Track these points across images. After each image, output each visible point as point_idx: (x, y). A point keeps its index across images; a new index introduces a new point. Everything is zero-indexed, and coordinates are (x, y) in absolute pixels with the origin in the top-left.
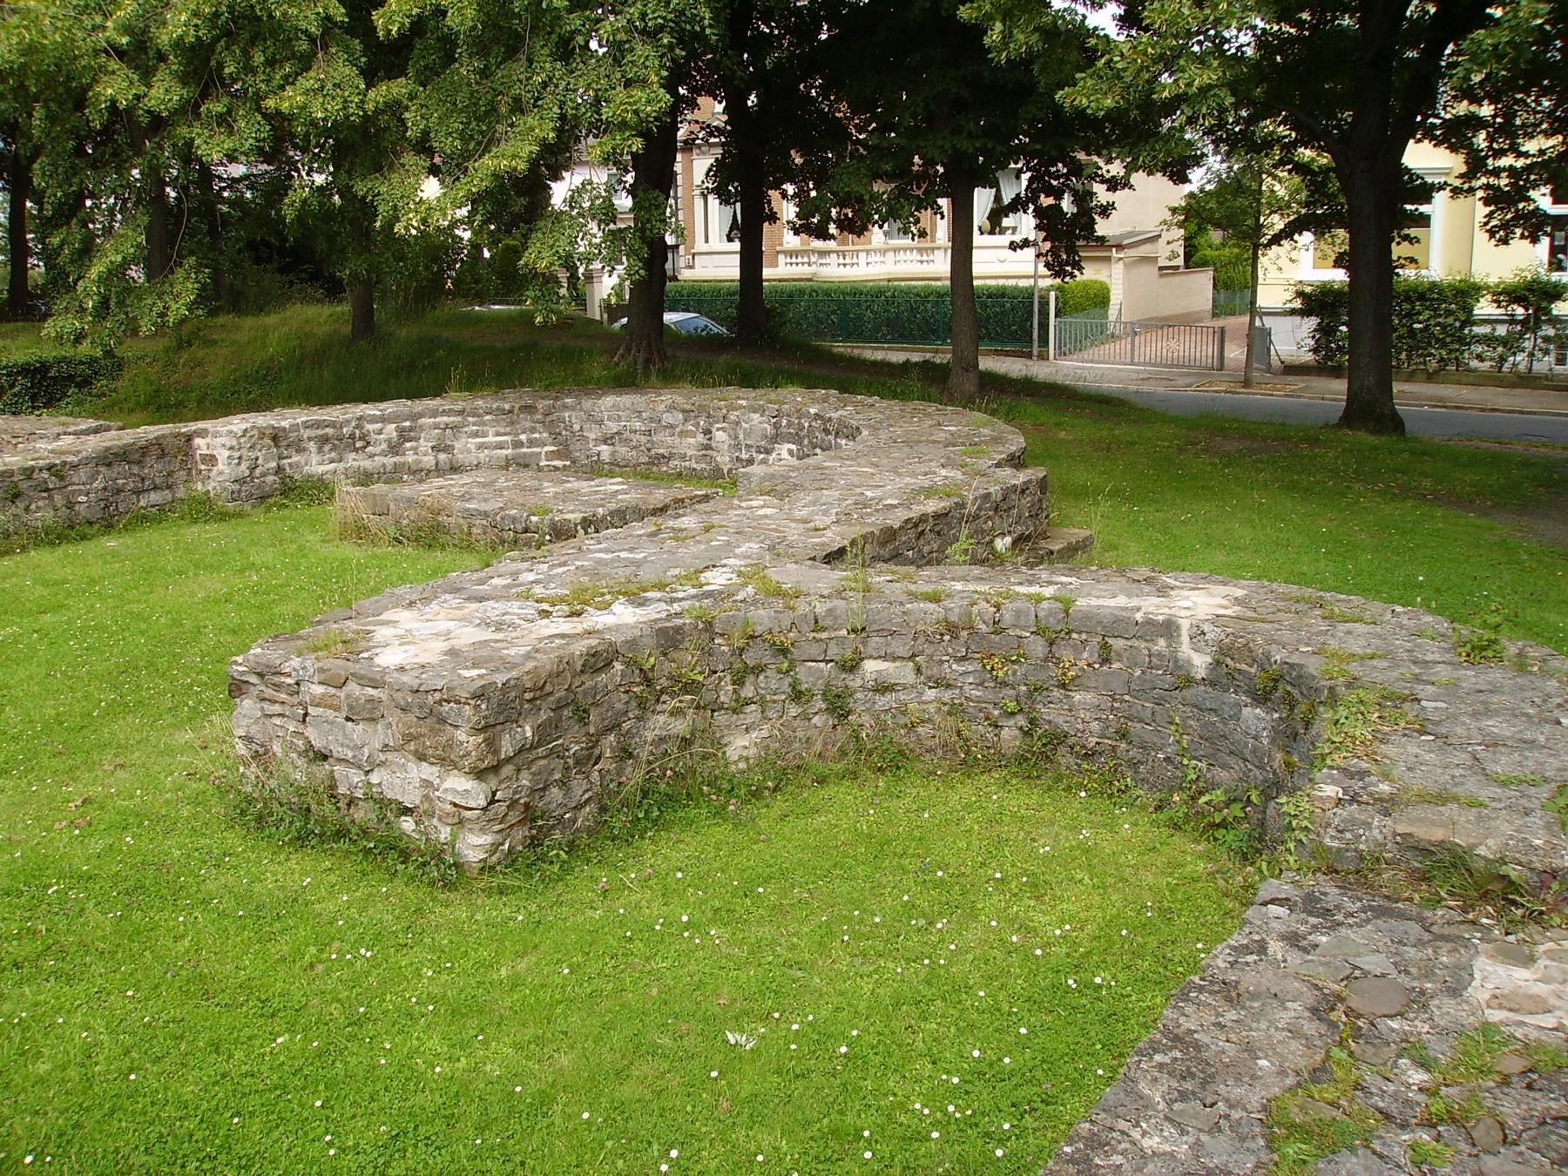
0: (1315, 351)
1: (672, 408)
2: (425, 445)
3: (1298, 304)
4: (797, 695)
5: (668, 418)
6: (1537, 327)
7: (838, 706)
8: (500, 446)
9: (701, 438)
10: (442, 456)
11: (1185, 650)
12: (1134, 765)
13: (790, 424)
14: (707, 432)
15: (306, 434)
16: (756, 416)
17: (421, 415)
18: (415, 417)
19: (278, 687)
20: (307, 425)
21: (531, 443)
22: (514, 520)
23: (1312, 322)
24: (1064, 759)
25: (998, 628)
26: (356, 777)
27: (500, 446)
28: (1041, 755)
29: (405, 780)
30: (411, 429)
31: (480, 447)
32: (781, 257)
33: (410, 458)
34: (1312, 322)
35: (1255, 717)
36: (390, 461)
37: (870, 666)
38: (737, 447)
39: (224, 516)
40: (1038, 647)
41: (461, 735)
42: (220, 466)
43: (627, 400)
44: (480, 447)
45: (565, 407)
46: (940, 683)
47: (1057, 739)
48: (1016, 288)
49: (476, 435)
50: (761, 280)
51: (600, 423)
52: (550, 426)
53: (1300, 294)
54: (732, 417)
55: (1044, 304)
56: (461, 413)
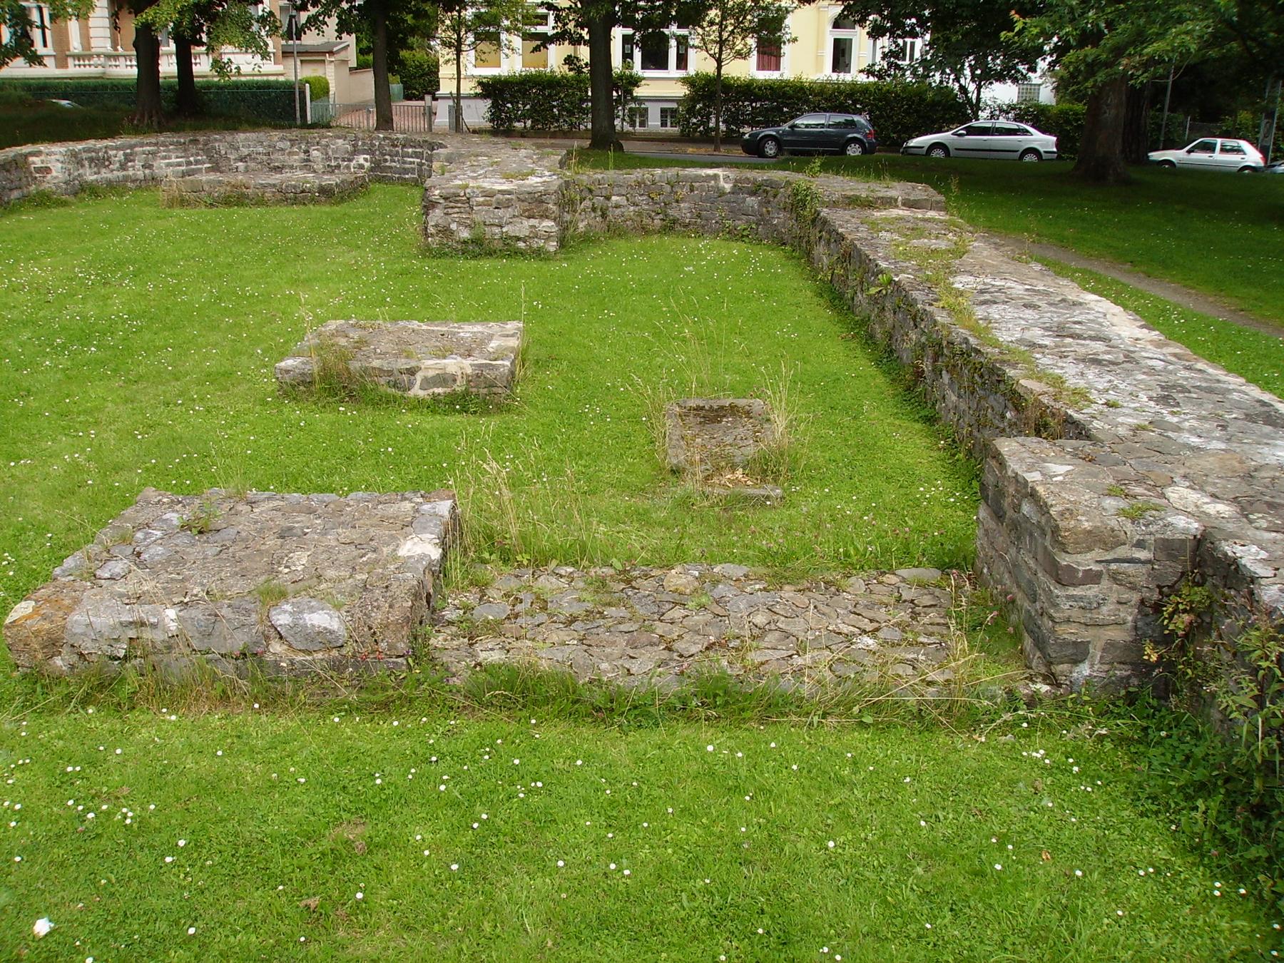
0: (491, 120)
1: (282, 139)
2: (138, 164)
3: (479, 90)
4: (594, 210)
5: (280, 145)
6: (626, 102)
7: (604, 216)
8: (179, 165)
9: (302, 155)
10: (147, 171)
11: (722, 183)
12: (703, 226)
13: (364, 144)
14: (306, 152)
15: (84, 155)
16: (340, 142)
17: (135, 146)
18: (132, 147)
19: (457, 202)
20: (85, 150)
21: (197, 162)
22: (295, 187)
23: (489, 102)
24: (678, 228)
25: (654, 183)
26: (497, 230)
27: (179, 165)
28: (670, 227)
29: (522, 227)
30: (131, 154)
31: (168, 165)
32: (70, 61)
33: (131, 172)
34: (489, 102)
35: (752, 201)
36: (121, 174)
37: (614, 198)
38: (329, 159)
39: (64, 204)
40: (668, 188)
41: (550, 206)
42: (54, 174)
43: (252, 136)
44: (168, 165)
45: (216, 140)
46: (635, 204)
47: (674, 221)
48: (277, 82)
49: (165, 158)
50: (138, 66)
51: (237, 149)
52: (207, 152)
53: (480, 83)
54: (324, 142)
55: (302, 93)
56: (156, 144)
